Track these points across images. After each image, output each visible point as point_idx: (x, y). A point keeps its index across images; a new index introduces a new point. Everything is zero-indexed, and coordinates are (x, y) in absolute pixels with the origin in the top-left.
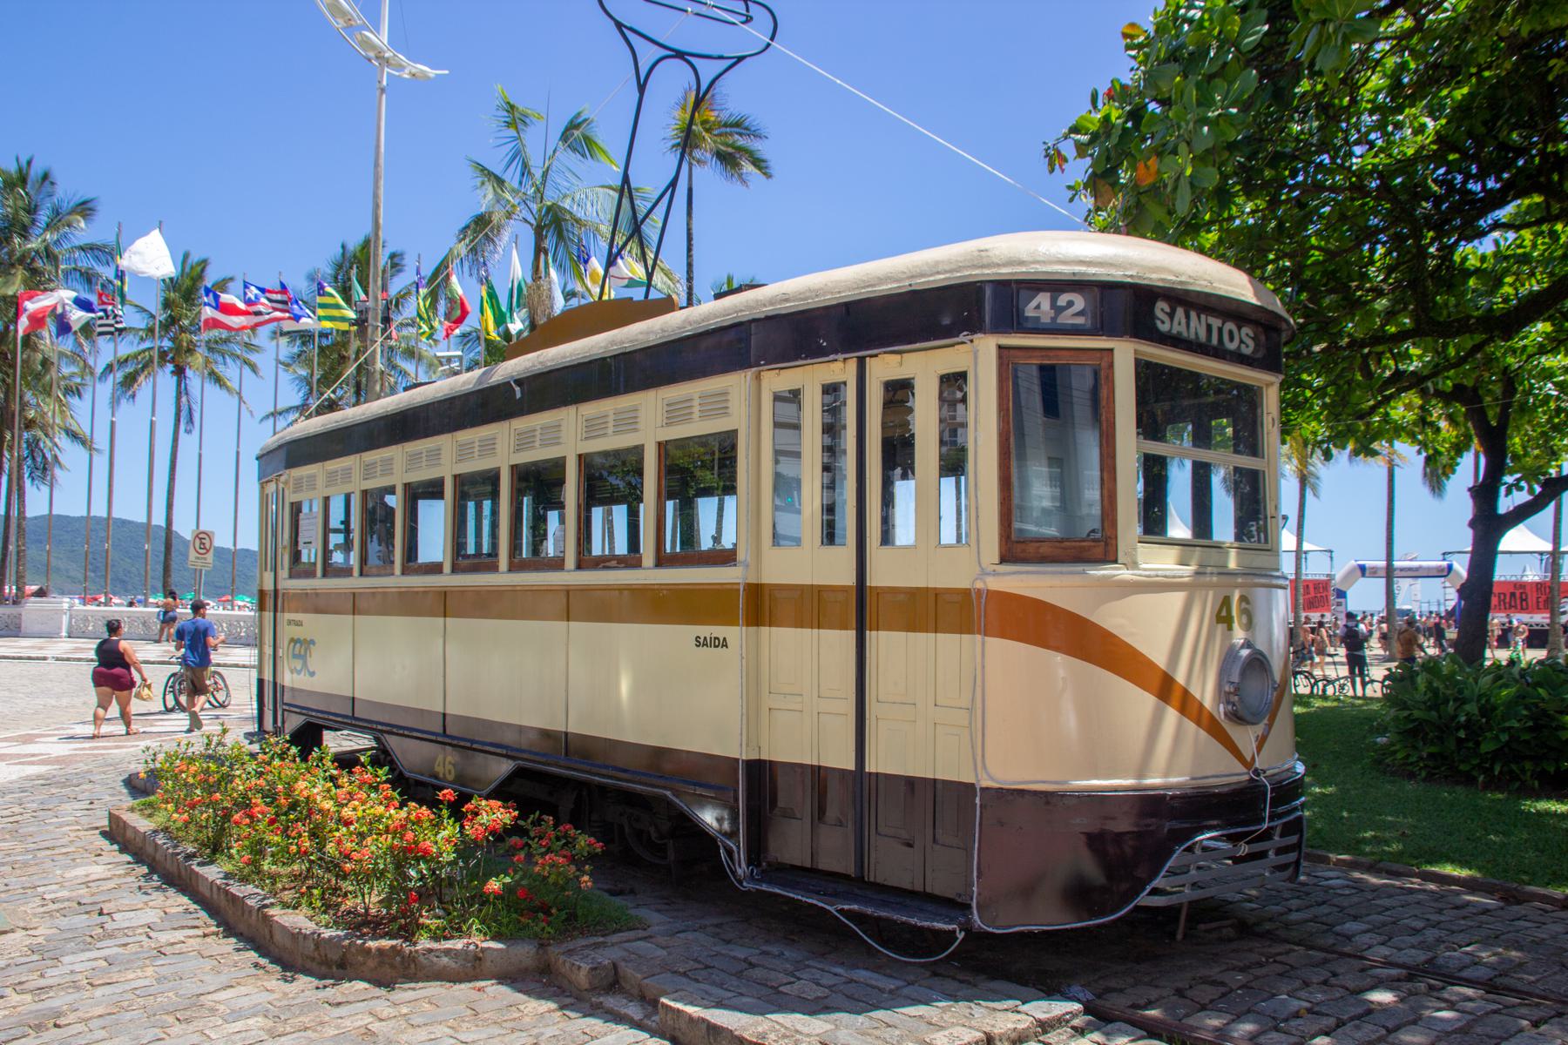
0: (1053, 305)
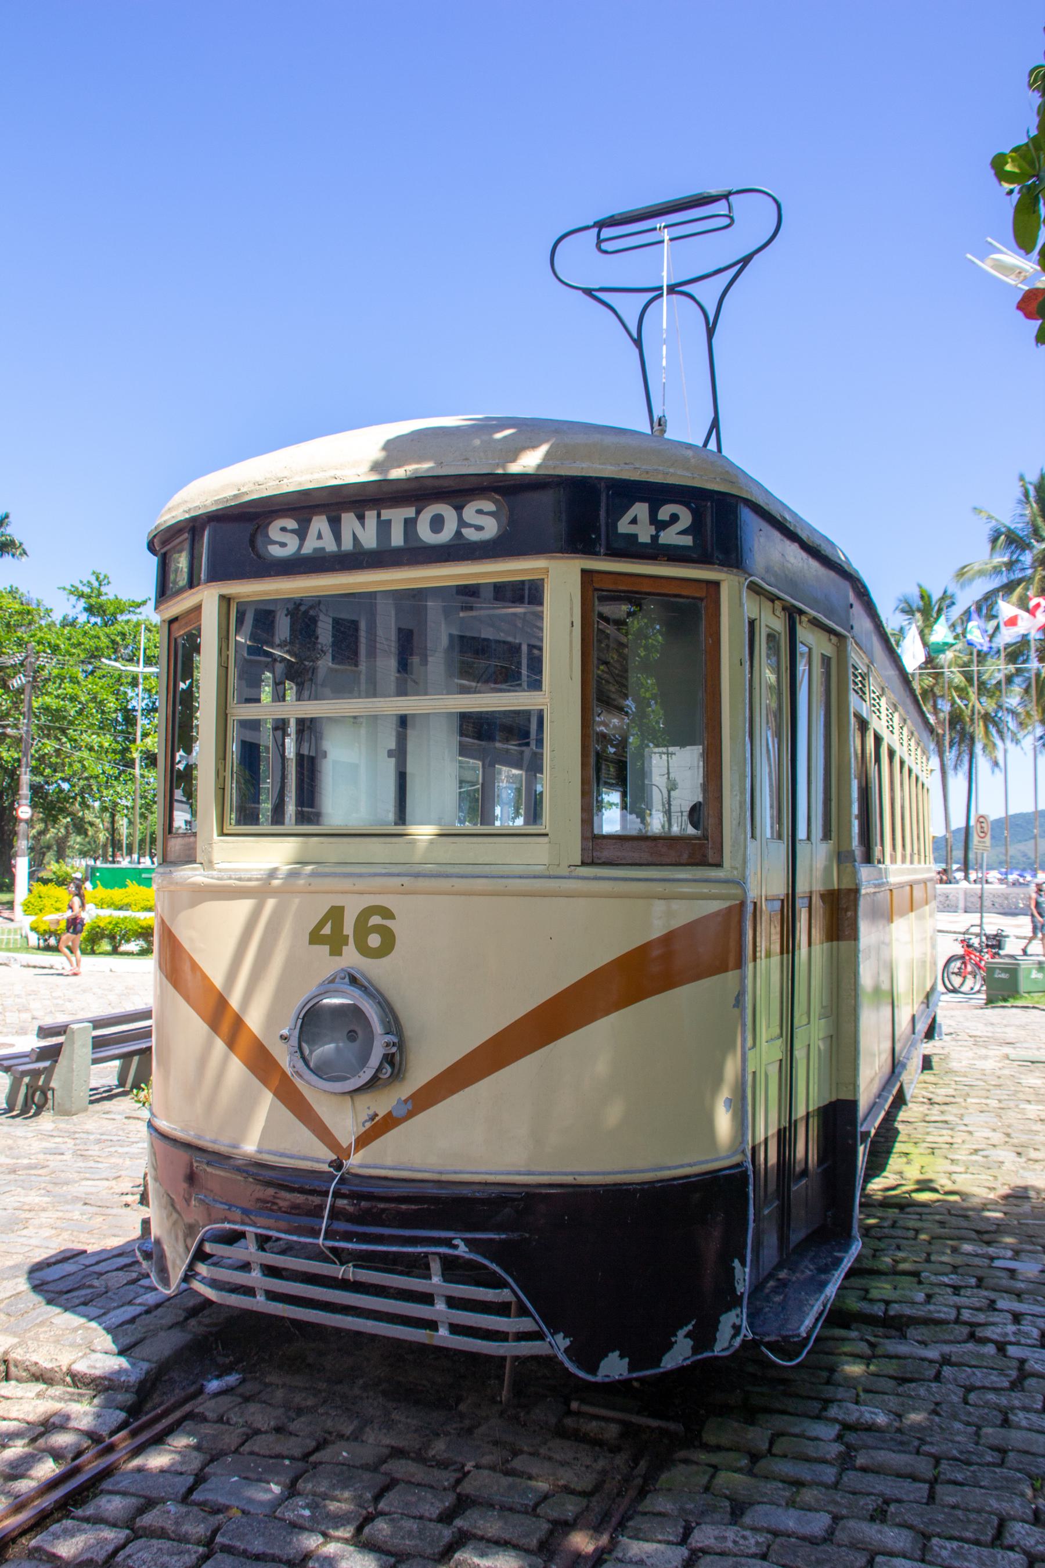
0: (653, 520)
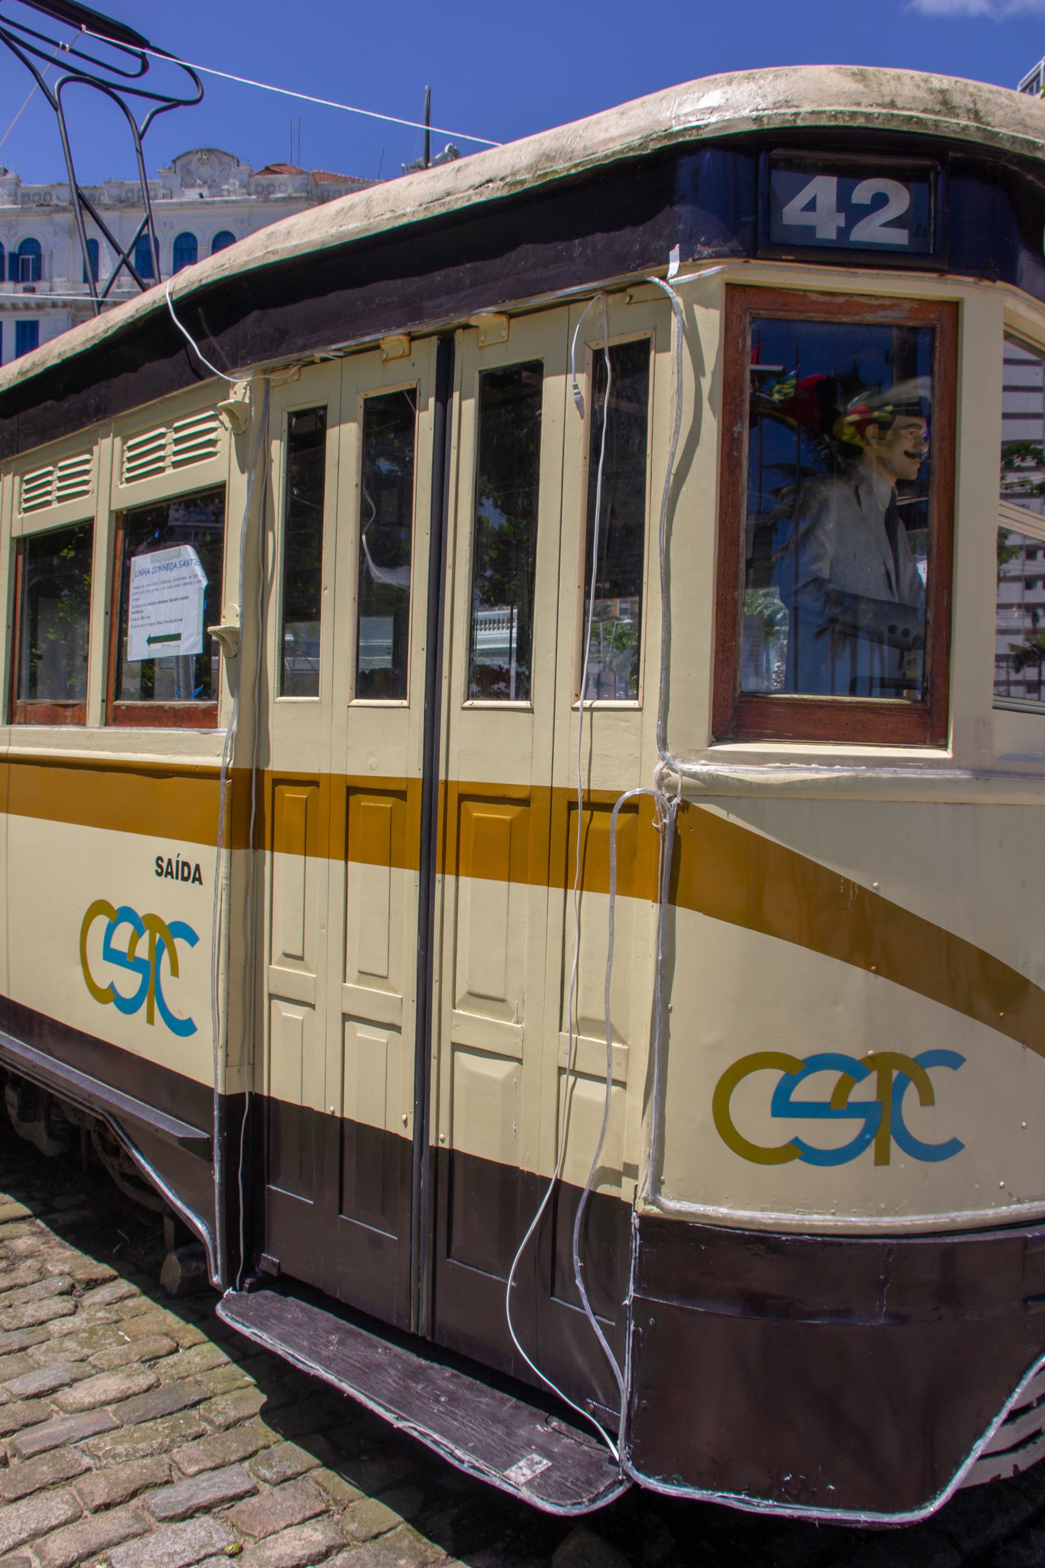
0: (843, 203)
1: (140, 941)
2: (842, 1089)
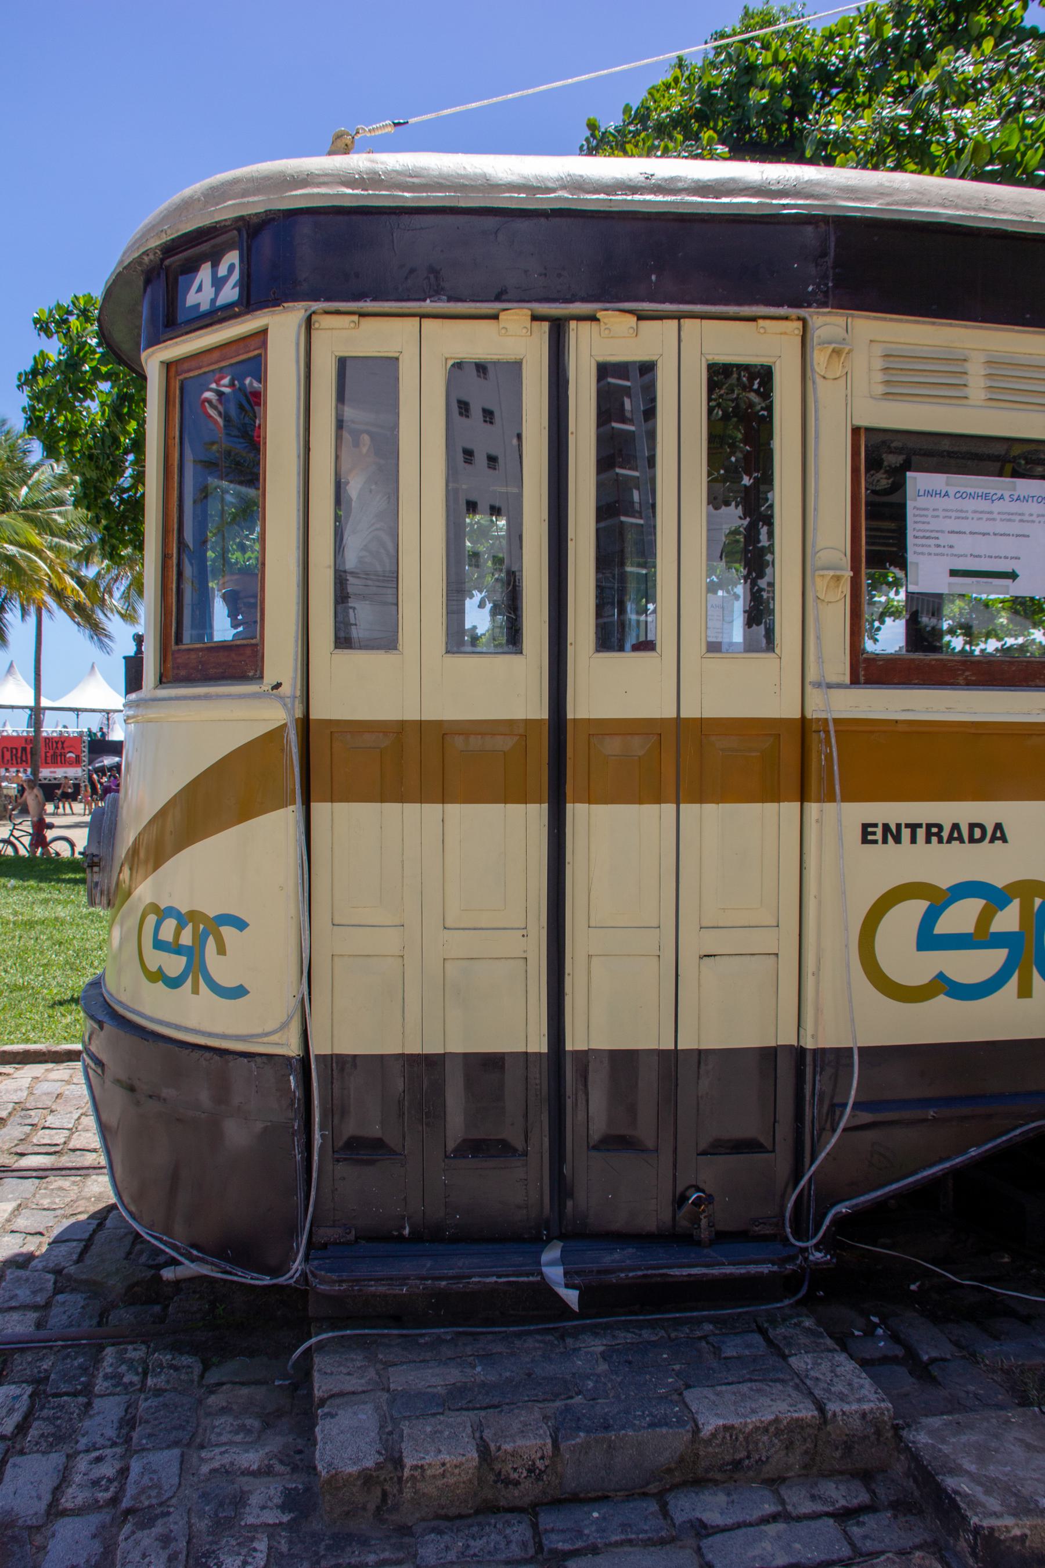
1: (183, 932)
2: (985, 918)
